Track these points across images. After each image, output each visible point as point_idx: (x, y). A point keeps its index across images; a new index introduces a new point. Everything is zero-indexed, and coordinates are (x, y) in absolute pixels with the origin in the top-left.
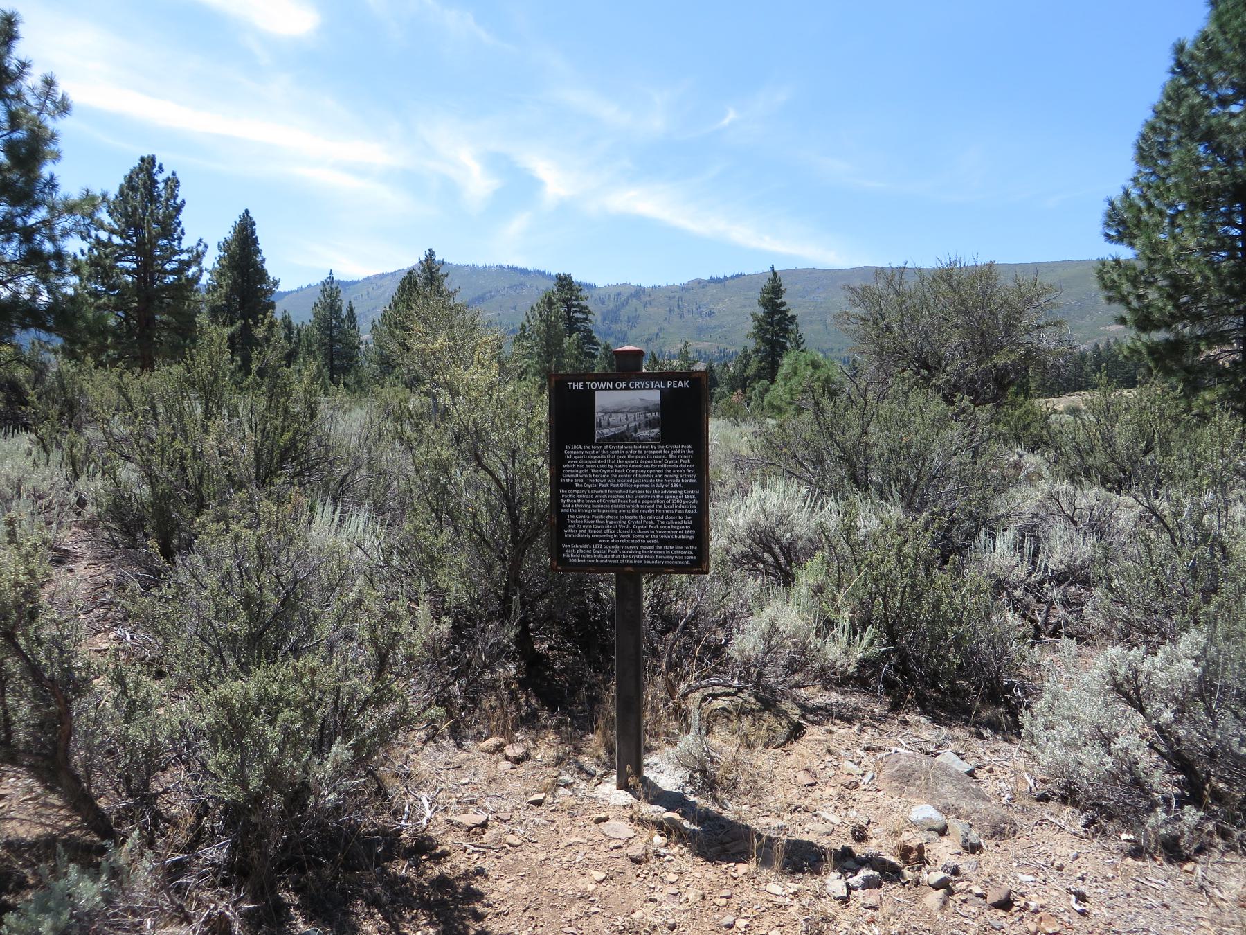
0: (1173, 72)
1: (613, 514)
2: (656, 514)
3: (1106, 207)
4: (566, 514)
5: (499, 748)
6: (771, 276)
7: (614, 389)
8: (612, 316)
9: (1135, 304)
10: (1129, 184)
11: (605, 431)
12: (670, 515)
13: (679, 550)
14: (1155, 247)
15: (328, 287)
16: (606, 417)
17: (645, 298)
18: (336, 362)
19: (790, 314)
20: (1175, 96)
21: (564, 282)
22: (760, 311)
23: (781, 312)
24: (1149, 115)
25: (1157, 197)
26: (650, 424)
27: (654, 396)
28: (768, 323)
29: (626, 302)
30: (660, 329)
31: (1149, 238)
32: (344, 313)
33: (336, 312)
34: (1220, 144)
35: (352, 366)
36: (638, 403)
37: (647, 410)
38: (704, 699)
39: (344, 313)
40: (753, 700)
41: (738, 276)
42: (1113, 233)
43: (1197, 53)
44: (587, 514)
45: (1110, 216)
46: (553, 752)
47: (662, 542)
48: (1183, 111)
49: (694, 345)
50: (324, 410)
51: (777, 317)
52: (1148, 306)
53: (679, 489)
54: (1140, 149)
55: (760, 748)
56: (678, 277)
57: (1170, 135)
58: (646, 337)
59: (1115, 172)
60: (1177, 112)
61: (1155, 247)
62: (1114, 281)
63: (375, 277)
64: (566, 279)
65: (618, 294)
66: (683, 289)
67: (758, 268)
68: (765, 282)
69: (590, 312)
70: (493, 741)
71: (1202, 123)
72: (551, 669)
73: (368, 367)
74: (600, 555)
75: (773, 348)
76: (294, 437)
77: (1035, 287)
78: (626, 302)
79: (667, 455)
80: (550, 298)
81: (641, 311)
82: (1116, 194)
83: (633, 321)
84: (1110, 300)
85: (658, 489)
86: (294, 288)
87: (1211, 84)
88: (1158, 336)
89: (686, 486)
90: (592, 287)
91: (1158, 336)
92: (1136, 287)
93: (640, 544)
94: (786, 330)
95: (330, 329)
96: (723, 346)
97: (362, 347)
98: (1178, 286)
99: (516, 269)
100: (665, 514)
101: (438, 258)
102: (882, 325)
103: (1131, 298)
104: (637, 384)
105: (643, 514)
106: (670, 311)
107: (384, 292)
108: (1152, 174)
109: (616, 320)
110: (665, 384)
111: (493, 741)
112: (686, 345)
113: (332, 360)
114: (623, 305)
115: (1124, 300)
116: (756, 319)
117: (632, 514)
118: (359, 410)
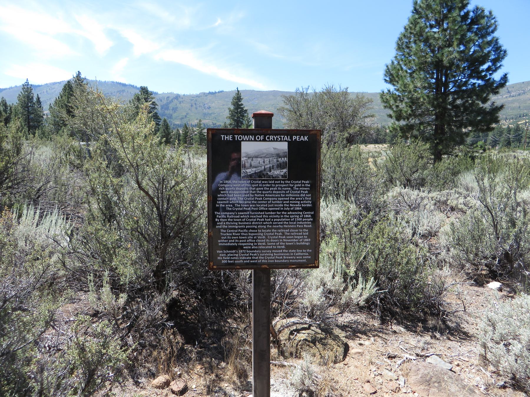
0: (413, 12)
1: (254, 229)
2: (284, 228)
3: (385, 68)
4: (220, 229)
5: (167, 384)
6: (237, 92)
7: (255, 140)
8: (166, 107)
9: (395, 109)
10: (394, 59)
11: (248, 171)
12: (293, 228)
13: (299, 252)
14: (405, 85)
15: (26, 87)
16: (249, 161)
17: (180, 100)
18: (31, 124)
19: (245, 109)
20: (414, 23)
21: (144, 90)
22: (232, 108)
23: (241, 108)
24: (403, 30)
25: (405, 65)
26: (280, 166)
27: (283, 146)
28: (236, 113)
29: (172, 101)
30: (187, 114)
31: (403, 81)
32: (35, 100)
33: (30, 99)
34: (430, 44)
35: (39, 126)
36: (272, 151)
37: (278, 156)
38: (291, 333)
39: (35, 100)
40: (320, 331)
41: (221, 92)
42: (388, 79)
43: (422, 5)
44: (235, 229)
45: (387, 72)
46: (202, 382)
47: (288, 247)
48: (418, 28)
49: (203, 121)
50: (26, 148)
51: (239, 110)
52: (401, 111)
53: (300, 211)
54: (398, 44)
55: (332, 364)
56: (195, 92)
57: (410, 39)
58: (181, 117)
59: (388, 54)
60: (415, 29)
61: (405, 85)
62: (387, 99)
63: (50, 84)
64: (145, 89)
65: (168, 97)
66: (197, 96)
67: (230, 88)
68: (234, 95)
69: (156, 104)
70: (161, 379)
71: (424, 34)
72: (183, 310)
73: (48, 127)
74: (240, 257)
75: (237, 123)
76: (6, 165)
77: (362, 101)
78: (172, 101)
79: (292, 188)
80: (138, 97)
81: (179, 105)
82: (389, 63)
83: (175, 109)
84: (385, 107)
85: (285, 211)
86: (8, 87)
87: (427, 19)
88: (402, 123)
89: (305, 209)
90: (156, 94)
91: (402, 123)
92: (396, 102)
93: (273, 249)
94: (243, 116)
95: (28, 107)
96: (215, 122)
97: (45, 117)
98: (414, 102)
99: (120, 84)
100: (290, 228)
101: (82, 76)
102: (298, 114)
103: (393, 107)
104: (271, 138)
105: (275, 229)
106: (192, 106)
107: (55, 91)
108: (402, 55)
109: (167, 109)
110: (291, 138)
111: (161, 379)
112: (200, 121)
113: (29, 123)
114: (170, 102)
115: (390, 107)
116: (230, 111)
117: (267, 228)
118: (44, 147)
